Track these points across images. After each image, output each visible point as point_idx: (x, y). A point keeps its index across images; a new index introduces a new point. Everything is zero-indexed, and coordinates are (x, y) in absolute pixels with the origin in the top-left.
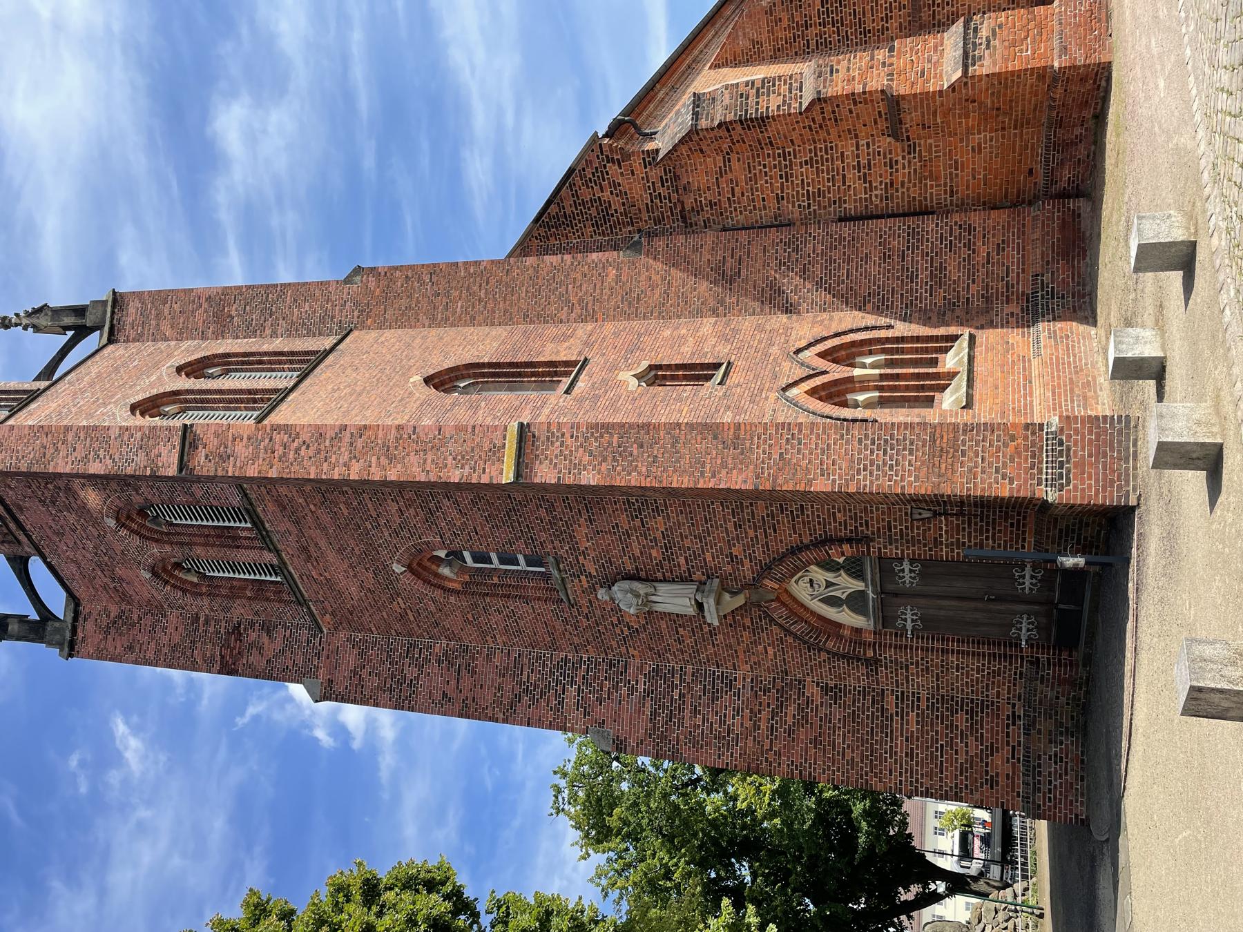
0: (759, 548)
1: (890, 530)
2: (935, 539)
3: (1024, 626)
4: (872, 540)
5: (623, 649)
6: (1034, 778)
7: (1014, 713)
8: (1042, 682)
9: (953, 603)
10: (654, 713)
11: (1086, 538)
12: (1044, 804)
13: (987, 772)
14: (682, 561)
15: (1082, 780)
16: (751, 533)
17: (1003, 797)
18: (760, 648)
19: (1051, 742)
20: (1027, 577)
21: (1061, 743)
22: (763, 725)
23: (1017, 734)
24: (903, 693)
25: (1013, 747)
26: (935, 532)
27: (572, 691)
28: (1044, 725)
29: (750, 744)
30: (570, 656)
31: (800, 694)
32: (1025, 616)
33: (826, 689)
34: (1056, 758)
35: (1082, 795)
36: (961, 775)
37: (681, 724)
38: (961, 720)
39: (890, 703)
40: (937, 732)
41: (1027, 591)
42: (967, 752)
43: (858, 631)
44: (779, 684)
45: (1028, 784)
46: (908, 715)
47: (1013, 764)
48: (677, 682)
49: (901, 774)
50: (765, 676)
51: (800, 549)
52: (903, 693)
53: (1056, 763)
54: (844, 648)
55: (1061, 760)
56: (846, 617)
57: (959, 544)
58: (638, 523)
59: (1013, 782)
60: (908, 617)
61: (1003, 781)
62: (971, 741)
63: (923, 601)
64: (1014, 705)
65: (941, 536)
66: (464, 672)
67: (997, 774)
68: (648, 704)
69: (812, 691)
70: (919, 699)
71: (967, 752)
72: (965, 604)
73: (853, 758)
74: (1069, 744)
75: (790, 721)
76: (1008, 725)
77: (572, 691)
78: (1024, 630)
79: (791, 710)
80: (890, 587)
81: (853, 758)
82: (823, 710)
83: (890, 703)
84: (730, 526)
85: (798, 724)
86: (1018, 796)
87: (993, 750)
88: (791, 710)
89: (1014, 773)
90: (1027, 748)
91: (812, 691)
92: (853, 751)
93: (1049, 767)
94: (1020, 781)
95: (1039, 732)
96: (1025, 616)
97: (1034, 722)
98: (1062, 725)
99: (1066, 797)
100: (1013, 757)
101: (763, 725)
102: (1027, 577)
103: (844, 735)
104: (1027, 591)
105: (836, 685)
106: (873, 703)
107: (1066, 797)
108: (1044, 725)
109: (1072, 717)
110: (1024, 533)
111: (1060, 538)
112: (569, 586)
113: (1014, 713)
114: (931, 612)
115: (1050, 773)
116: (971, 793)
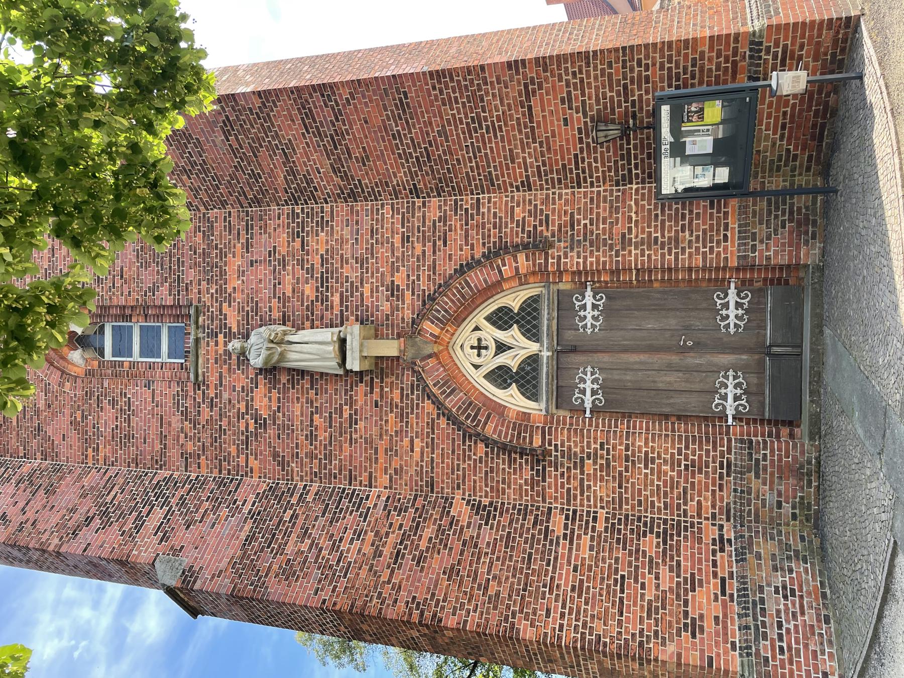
0: (424, 272)
1: (573, 229)
2: (624, 235)
3: (731, 391)
4: (551, 246)
5: (242, 460)
6: (755, 619)
7: (721, 537)
8: (757, 476)
9: (643, 357)
10: (250, 539)
11: (799, 209)
12: (774, 658)
13: (686, 613)
14: (336, 299)
15: (827, 622)
16: (419, 248)
17: (710, 649)
18: (406, 441)
19: (775, 569)
20: (732, 305)
21: (791, 571)
22: (387, 551)
23: (726, 562)
24: (575, 512)
25: (723, 580)
26: (623, 226)
27: (159, 513)
28: (765, 547)
29: (363, 574)
30: (176, 475)
31: (445, 512)
32: (731, 373)
33: (477, 508)
34: (786, 592)
35: (830, 642)
36: (649, 617)
37: (281, 550)
38: (650, 544)
39: (557, 524)
40: (617, 559)
41: (732, 330)
42: (657, 587)
43: (526, 416)
44: (420, 502)
45: (747, 627)
46: (579, 536)
47: (724, 602)
48: (294, 501)
49: (562, 615)
50: (405, 493)
51: (469, 266)
52: (575, 512)
53: (785, 597)
54: (506, 436)
55: (793, 593)
56: (512, 398)
57: (652, 242)
58: (297, 244)
59: (725, 628)
60: (588, 387)
61: (709, 626)
62: (664, 571)
63: (605, 358)
64: (721, 527)
65: (630, 229)
66: (42, 492)
67: (701, 616)
68: (247, 528)
69: (461, 510)
70: (595, 519)
71: (657, 587)
72: (658, 359)
73: (498, 594)
74: (804, 574)
75: (423, 545)
76: (714, 553)
77: (159, 513)
78: (730, 398)
79: (429, 532)
80: (569, 335)
81: (498, 594)
82: (472, 532)
83: (557, 524)
84: (397, 239)
85: (432, 548)
86: (734, 647)
87: (693, 584)
88: (429, 532)
89: (725, 616)
90: (742, 579)
91: (461, 510)
92: (500, 583)
93: (775, 604)
94: (734, 627)
95: (759, 556)
96: (731, 373)
97: (751, 544)
98: (788, 547)
99: (806, 646)
100: (723, 593)
101: (387, 551)
102: (732, 305)
103: (491, 563)
104: (732, 330)
105: (491, 504)
106: (535, 523)
107: (806, 646)
108: (765, 547)
109: (802, 538)
110: (726, 213)
111: (769, 213)
112: (202, 352)
113: (721, 537)
114: (616, 376)
115: (778, 612)
116: (664, 644)
